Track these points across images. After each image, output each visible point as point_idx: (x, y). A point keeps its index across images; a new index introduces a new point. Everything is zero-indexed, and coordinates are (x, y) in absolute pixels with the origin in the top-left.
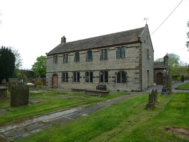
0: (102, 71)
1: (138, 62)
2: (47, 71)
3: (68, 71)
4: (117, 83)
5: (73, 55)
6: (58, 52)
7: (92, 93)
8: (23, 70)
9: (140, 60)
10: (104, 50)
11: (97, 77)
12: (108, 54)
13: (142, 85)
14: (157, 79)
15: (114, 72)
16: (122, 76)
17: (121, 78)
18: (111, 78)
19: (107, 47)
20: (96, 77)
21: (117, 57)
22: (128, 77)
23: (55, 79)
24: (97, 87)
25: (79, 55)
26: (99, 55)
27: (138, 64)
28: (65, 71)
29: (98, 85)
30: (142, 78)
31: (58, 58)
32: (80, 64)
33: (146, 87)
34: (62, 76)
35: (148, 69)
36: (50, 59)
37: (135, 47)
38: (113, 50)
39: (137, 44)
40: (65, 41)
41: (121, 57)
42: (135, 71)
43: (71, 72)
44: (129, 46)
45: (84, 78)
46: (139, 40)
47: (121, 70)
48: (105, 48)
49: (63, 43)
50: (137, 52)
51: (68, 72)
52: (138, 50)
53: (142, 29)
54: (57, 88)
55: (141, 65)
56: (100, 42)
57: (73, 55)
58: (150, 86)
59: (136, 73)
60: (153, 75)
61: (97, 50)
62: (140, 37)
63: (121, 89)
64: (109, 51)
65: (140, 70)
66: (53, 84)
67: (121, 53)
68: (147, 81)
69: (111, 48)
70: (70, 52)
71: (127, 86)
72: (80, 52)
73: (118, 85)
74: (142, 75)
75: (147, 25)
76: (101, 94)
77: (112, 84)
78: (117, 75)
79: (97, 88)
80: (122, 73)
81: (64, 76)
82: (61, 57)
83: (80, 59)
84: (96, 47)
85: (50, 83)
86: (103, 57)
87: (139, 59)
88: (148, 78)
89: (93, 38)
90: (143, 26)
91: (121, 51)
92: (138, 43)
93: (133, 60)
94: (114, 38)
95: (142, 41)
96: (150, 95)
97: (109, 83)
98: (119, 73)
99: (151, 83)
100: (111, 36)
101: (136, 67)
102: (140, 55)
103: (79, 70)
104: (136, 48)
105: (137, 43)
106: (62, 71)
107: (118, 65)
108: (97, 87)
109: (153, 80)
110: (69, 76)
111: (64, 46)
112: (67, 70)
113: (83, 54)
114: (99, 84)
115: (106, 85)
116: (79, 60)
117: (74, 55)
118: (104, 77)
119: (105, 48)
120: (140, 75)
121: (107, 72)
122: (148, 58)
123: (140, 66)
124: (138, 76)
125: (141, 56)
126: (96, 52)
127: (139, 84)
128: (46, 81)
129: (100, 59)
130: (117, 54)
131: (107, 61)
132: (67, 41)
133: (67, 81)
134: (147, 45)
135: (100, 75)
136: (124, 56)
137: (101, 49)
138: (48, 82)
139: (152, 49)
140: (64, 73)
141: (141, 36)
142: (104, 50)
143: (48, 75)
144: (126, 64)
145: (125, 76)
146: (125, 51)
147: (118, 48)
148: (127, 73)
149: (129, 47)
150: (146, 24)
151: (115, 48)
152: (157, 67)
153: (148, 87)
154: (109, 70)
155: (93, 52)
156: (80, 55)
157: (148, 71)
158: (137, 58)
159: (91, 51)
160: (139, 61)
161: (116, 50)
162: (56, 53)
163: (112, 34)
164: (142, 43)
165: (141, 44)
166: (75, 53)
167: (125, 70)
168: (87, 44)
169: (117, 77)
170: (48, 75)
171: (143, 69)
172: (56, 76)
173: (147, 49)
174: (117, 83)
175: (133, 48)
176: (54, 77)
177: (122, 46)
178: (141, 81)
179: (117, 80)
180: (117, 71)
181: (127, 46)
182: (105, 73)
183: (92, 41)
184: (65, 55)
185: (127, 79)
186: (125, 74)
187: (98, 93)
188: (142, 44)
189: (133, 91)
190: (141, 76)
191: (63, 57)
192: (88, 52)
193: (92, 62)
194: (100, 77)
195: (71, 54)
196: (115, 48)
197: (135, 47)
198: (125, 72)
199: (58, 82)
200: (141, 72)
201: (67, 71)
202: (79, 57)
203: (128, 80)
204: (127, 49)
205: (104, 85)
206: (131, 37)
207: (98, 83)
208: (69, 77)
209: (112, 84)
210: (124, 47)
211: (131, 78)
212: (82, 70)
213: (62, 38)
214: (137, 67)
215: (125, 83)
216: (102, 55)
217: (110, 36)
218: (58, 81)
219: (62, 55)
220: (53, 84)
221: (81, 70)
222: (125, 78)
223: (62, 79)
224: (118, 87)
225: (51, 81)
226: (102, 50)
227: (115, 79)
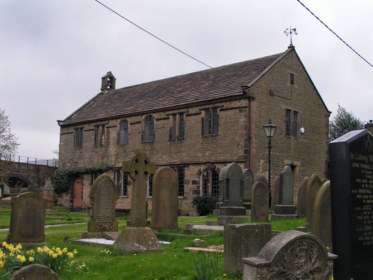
5: (116, 126)
8: (23, 164)
10: (178, 116)
31: (85, 133)
37: (236, 108)
40: (112, 87)
44: (226, 105)
46: (245, 93)
57: (116, 126)
61: (163, 115)
66: (72, 201)
70: (108, 119)
90: (283, 49)
97: (185, 195)
104: (240, 111)
105: (240, 99)
117: (118, 125)
119: (181, 111)
132: (119, 85)
142: (178, 116)
150: (289, 45)
154: (187, 165)
155: (157, 120)
169: (201, 182)
191: (93, 132)
192: (146, 120)
213: (103, 79)
219: (92, 126)
220: (72, 201)
227: (199, 187)
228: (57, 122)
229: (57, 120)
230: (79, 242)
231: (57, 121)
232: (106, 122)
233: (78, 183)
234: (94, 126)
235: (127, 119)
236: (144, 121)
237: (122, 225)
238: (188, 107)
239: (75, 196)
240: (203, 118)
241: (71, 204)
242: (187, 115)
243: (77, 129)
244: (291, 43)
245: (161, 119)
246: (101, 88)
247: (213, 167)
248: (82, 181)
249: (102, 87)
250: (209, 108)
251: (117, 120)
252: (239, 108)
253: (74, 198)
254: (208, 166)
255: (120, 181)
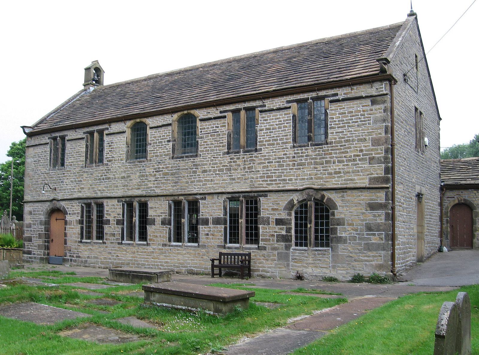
0: (233, 197)
1: (379, 162)
2: (27, 198)
3: (105, 194)
4: (293, 247)
5: (124, 132)
6: (68, 123)
7: (174, 298)
9: (386, 151)
10: (243, 113)
11: (217, 221)
12: (258, 128)
13: (396, 256)
14: (452, 227)
15: (284, 200)
16: (316, 217)
17: (311, 226)
18: (273, 225)
19: (255, 100)
20: (211, 221)
21: (295, 140)
22: (340, 222)
23: (56, 226)
24: (213, 260)
25: (146, 134)
26: (225, 130)
27: (379, 171)
28: (94, 195)
29: (221, 254)
30: (397, 224)
31: (68, 145)
32: (150, 170)
33: (411, 259)
34: (82, 217)
35: (418, 189)
36: (39, 150)
38: (279, 109)
39: (377, 85)
40: (98, 82)
41: (310, 139)
42: (366, 197)
43: (115, 202)
44: (342, 93)
45: (163, 223)
46: (383, 71)
47: (311, 192)
48: (247, 105)
49: (92, 89)
50: (375, 122)
51: (105, 202)
52: (378, 111)
53: (395, 29)
54: (65, 261)
55: (393, 173)
56: (228, 80)
57: (124, 132)
58: (425, 253)
59: (373, 207)
60: (438, 212)
61: (214, 112)
62: (386, 59)
63: (309, 270)
64: (264, 115)
65: (390, 196)
66: (47, 248)
67: (310, 122)
68: (416, 237)
69: (270, 104)
71: (336, 259)
72: (150, 122)
73: (297, 253)
74: (397, 213)
75: (412, 14)
76: (211, 305)
77: (274, 249)
78: (296, 213)
79: (213, 266)
80: (316, 204)
81: (89, 217)
82: (79, 143)
83: (149, 148)
84: (212, 98)
85: (38, 242)
86: (238, 140)
87: (383, 147)
88: (420, 225)
89: (204, 66)
91: (310, 113)
92: (381, 81)
93: (361, 151)
94: (283, 64)
95: (398, 75)
96: (439, 337)
97: (261, 244)
98: (303, 205)
99: (428, 243)
100: (272, 59)
101: (370, 179)
102: (386, 132)
103: (144, 193)
104: (373, 103)
105: (373, 82)
106: (80, 195)
107: (299, 172)
108: (216, 263)
109: (436, 230)
110: (106, 217)
111: (94, 97)
112: (102, 191)
113: (159, 129)
114: (224, 247)
115: (249, 255)
116: (146, 151)
117: (129, 131)
118: (242, 221)
119: (247, 105)
120: (387, 214)
121: (256, 202)
122: (419, 145)
123: (390, 176)
124: (380, 217)
125: (392, 138)
126: (210, 119)
127: (384, 249)
128: (26, 235)
129: (229, 148)
130: (295, 127)
131: (255, 154)
132: (108, 80)
133: (100, 236)
134: (417, 93)
135: (225, 214)
136: (323, 137)
137: (232, 107)
138: (30, 239)
139: (432, 110)
140: (89, 205)
141: (391, 56)
142: (243, 113)
143: (30, 213)
144: (332, 168)
145: (327, 217)
146: (326, 114)
147: (298, 101)
148: (335, 207)
149: (344, 100)
150: (409, 12)
151: (288, 102)
152: (453, 178)
153: (420, 260)
154: (265, 193)
155: (202, 120)
156: (149, 131)
157: (419, 196)
158: (376, 142)
159: (191, 114)
160: (386, 158)
161: (290, 111)
162: (61, 125)
163: (276, 52)
164: (396, 81)
165: (390, 85)
166: (129, 123)
167: (327, 195)
168: (179, 89)
170: (30, 213)
171: (398, 188)
172: (59, 216)
173: (416, 109)
174: (293, 247)
175: (358, 102)
176: (53, 222)
177: (314, 94)
178: (393, 238)
179: (296, 232)
180: (296, 198)
181: (336, 95)
182: (247, 203)
183: (199, 77)
184: (92, 133)
185: (334, 231)
186: (328, 211)
187: (197, 302)
188: (395, 87)
189: (358, 279)
190: (392, 217)
191: (83, 143)
193: (197, 160)
194: (225, 220)
195: (115, 127)
196: (288, 102)
197: (367, 97)
198: (329, 199)
199: (65, 241)
200: (393, 200)
201: (99, 195)
202: (145, 140)
203: (341, 232)
204: (333, 106)
205: (242, 255)
206: (351, 59)
207: (219, 246)
208: (108, 222)
209: (274, 249)
210: (323, 98)
211: (352, 224)
212: (158, 191)
213: (88, 69)
214: (377, 180)
215: (328, 245)
216: (237, 131)
217: (271, 56)
218: (65, 235)
219: (80, 133)
221: (152, 193)
222: (327, 224)
223: (82, 228)
224: (301, 261)
225: (40, 236)
226: (236, 112)
227: (289, 230)
228: (22, 128)
229: (22, 126)
230: (376, 294)
231: (21, 127)
232: (106, 126)
233: (56, 220)
234: (84, 133)
235: (144, 121)
236: (176, 122)
237: (438, 262)
238: (264, 98)
239: (52, 240)
240: (294, 116)
241: (46, 251)
242: (261, 111)
243: (55, 139)
244: (412, 8)
245: (210, 119)
246: (83, 82)
247: (318, 196)
248: (66, 218)
249: (85, 82)
250: (308, 99)
251: (125, 122)
252: (371, 96)
253: (51, 243)
254: (308, 195)
255: (134, 218)
